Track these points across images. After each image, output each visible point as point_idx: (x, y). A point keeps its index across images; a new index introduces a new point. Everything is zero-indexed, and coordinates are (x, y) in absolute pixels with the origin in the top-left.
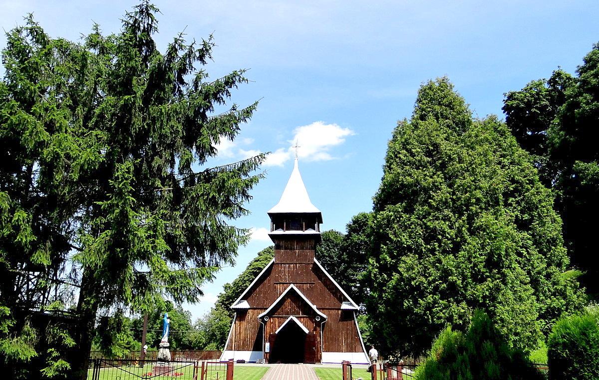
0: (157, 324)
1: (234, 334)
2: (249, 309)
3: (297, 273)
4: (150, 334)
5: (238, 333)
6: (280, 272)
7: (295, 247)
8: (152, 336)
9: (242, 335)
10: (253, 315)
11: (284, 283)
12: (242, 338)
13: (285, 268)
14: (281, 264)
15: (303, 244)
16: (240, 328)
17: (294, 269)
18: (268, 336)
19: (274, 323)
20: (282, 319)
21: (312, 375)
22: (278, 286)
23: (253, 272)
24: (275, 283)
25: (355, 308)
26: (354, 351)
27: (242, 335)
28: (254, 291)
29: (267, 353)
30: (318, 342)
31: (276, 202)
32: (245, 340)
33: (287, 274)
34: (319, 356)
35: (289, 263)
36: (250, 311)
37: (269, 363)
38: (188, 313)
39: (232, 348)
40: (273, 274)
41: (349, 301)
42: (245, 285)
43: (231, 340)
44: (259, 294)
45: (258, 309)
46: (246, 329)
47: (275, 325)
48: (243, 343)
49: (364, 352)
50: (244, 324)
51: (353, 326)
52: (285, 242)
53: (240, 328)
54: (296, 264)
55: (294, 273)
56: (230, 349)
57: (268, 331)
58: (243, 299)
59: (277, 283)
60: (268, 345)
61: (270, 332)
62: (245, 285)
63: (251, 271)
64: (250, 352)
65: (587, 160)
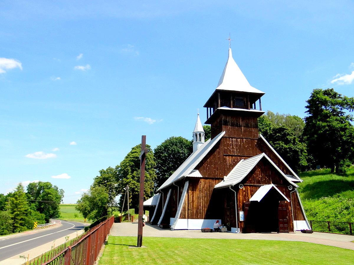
0: (40, 198)
1: (187, 202)
2: (201, 178)
3: (244, 147)
4: (34, 204)
5: (191, 201)
6: (228, 145)
7: (241, 123)
8: (36, 206)
9: (195, 203)
10: (205, 184)
11: (232, 156)
12: (195, 206)
13: (232, 141)
14: (229, 138)
15: (248, 121)
16: (193, 196)
17: (241, 143)
18: (241, 204)
19: (246, 191)
20: (254, 187)
21: (49, 225)
22: (228, 158)
23: (133, 160)
24: (224, 155)
25: (298, 181)
26: (202, 218)
27: (195, 203)
28: (205, 162)
29: (241, 222)
30: (289, 211)
31: (220, 82)
32: (197, 208)
33: (235, 147)
34: (291, 224)
35: (236, 136)
36: (202, 180)
37: (242, 233)
38: (62, 190)
39: (185, 215)
40: (221, 147)
41: (293, 175)
42: (127, 169)
43: (184, 208)
44: (211, 165)
45: (210, 178)
46: (198, 198)
47: (248, 193)
48: (197, 211)
49: (305, 219)
50: (197, 193)
51: (295, 197)
52: (231, 118)
53: (193, 196)
54: (237, 138)
55: (241, 146)
56: (183, 217)
57: (241, 199)
58: (197, 168)
59: (227, 156)
60: (241, 213)
61: (243, 201)
62: (127, 169)
63: (131, 159)
64: (202, 220)
65: (310, 116)
